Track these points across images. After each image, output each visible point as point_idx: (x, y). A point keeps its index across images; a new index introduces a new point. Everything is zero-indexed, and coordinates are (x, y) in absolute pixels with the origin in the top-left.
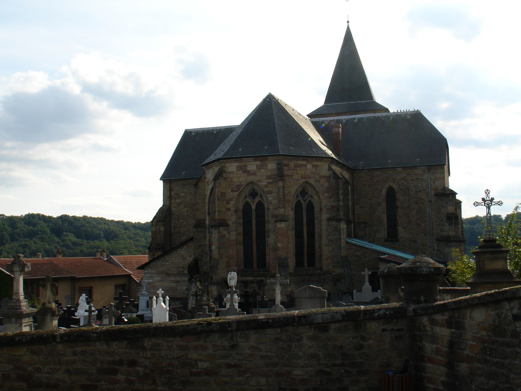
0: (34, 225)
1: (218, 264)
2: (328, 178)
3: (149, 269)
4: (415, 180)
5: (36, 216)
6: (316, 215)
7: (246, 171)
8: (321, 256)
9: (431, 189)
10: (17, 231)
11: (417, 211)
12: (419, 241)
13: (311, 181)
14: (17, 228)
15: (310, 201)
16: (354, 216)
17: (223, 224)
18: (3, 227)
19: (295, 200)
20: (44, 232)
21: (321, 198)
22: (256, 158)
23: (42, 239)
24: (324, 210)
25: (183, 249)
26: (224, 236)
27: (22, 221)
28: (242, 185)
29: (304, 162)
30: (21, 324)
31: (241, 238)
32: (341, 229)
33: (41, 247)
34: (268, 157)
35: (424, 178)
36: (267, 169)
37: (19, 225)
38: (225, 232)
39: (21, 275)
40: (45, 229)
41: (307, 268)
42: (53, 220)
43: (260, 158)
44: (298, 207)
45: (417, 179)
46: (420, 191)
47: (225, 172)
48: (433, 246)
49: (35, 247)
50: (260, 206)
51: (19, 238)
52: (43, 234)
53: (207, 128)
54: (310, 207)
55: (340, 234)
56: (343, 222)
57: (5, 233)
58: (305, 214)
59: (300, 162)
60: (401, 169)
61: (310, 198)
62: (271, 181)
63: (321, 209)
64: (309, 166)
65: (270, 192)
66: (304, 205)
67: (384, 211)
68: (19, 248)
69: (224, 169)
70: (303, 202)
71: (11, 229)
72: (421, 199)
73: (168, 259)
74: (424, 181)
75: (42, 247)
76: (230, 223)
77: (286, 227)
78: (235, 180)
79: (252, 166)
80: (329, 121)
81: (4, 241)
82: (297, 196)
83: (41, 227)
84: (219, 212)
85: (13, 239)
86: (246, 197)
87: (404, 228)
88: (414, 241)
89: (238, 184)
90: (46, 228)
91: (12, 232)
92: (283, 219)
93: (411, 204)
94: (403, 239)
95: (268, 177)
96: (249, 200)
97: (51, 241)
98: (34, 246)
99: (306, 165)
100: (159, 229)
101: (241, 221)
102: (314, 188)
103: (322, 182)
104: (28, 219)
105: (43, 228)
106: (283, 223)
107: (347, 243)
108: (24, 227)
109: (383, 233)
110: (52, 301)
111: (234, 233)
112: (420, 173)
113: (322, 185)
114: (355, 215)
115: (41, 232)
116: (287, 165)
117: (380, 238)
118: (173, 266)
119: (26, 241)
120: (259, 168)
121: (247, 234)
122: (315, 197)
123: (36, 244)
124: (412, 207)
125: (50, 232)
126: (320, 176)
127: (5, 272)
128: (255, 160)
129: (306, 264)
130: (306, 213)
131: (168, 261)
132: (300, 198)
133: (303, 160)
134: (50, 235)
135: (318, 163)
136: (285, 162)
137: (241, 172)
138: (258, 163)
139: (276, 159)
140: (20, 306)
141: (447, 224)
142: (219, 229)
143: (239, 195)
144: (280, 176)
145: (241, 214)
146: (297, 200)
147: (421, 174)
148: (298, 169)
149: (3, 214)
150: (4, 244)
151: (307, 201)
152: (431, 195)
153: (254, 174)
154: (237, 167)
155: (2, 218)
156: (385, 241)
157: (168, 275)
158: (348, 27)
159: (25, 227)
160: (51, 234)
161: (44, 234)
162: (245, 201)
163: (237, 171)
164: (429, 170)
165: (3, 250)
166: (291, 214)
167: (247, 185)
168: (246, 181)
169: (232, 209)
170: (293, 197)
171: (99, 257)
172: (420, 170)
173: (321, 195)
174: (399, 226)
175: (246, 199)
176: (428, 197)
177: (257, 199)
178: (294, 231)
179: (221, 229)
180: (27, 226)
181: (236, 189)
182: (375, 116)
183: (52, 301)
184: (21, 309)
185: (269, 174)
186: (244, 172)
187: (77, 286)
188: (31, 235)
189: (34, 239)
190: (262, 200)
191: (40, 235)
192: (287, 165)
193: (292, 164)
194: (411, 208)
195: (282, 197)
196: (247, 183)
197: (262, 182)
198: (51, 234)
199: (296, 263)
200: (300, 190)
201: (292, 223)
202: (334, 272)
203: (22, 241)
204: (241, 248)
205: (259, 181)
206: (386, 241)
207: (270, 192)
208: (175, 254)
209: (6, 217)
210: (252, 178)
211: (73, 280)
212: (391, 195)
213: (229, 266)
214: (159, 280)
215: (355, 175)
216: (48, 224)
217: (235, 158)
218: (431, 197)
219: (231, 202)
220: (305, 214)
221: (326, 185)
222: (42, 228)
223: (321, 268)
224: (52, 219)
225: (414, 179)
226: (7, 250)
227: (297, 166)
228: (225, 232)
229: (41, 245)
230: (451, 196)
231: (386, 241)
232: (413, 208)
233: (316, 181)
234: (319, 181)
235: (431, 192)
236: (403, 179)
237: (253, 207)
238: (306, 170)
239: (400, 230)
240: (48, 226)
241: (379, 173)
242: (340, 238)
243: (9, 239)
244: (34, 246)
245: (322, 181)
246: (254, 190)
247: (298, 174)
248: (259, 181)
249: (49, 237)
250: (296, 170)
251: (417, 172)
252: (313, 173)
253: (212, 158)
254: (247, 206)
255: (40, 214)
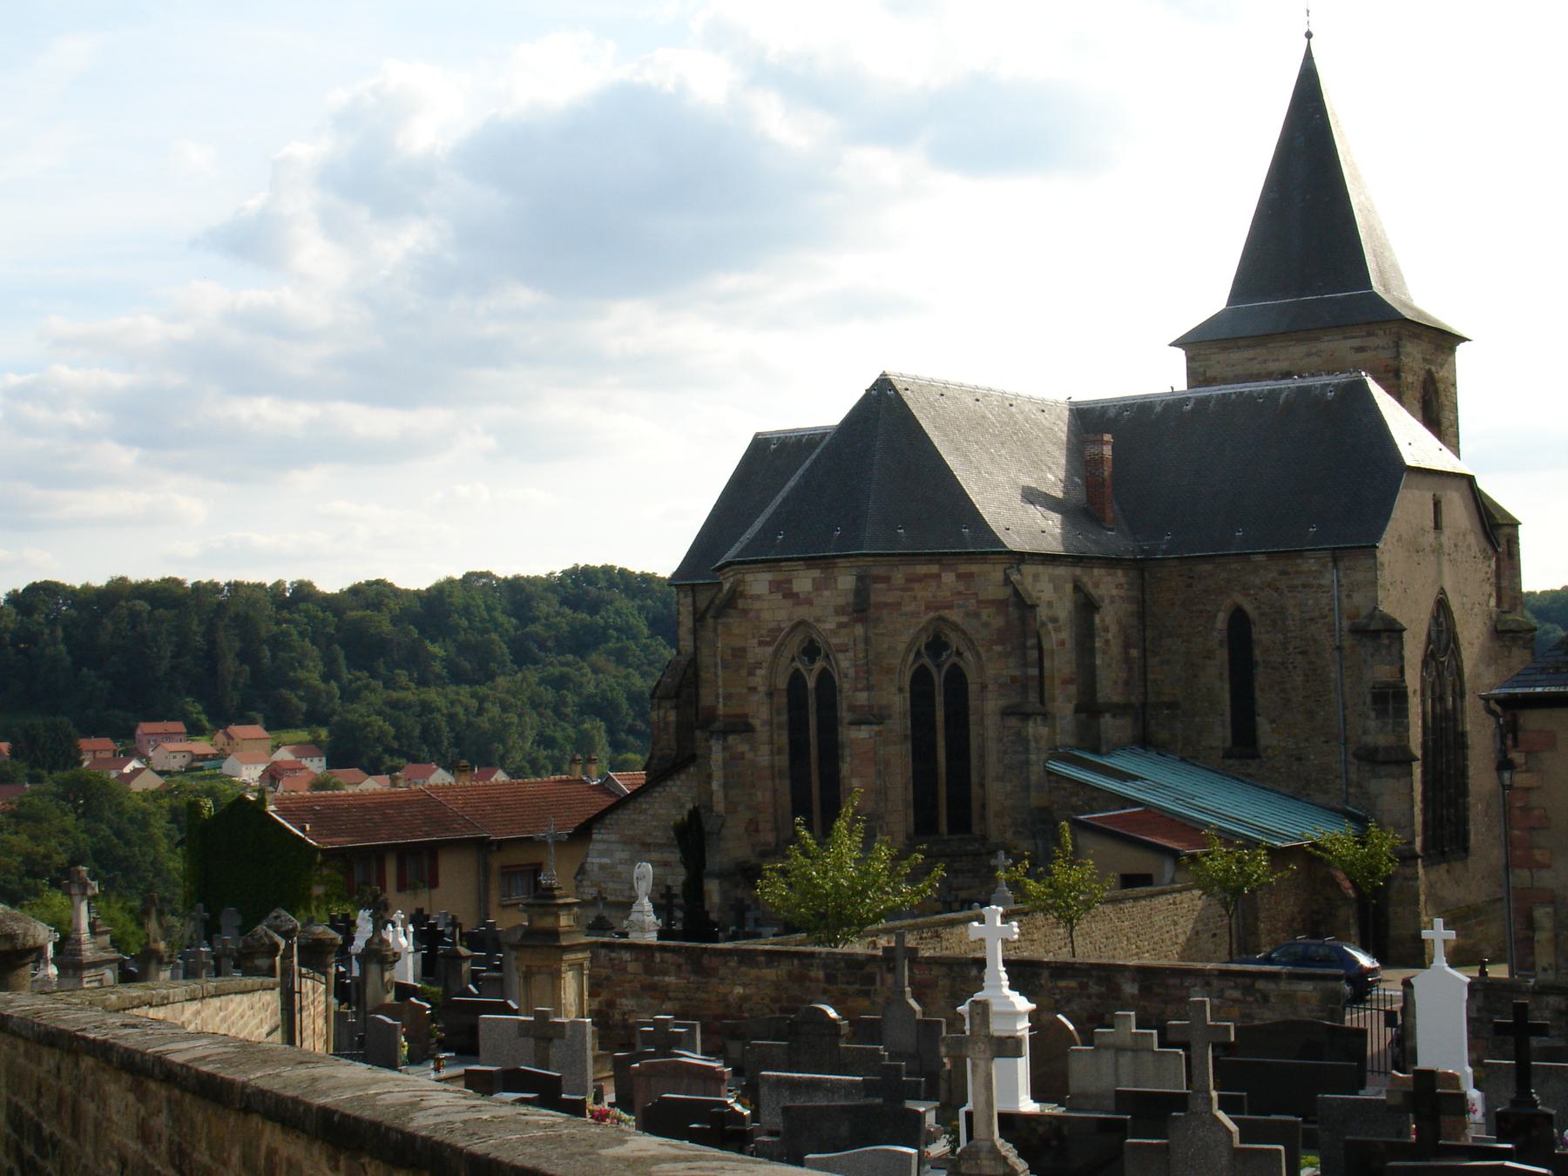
0: (594, 607)
1: (722, 825)
2: (1001, 605)
3: (602, 831)
4: (1300, 589)
5: (601, 575)
6: (973, 702)
7: (790, 595)
8: (983, 807)
9: (1340, 614)
10: (537, 628)
11: (1306, 675)
12: (1312, 757)
13: (954, 616)
14: (535, 619)
15: (955, 666)
16: (1146, 686)
17: (741, 726)
18: (487, 617)
19: (912, 665)
20: (626, 631)
21: (984, 656)
22: (811, 562)
23: (620, 657)
24: (990, 687)
25: (679, 783)
26: (742, 756)
27: (550, 595)
28: (780, 630)
29: (934, 569)
30: (81, 979)
31: (783, 761)
32: (1031, 737)
33: (615, 685)
34: (837, 561)
35: (1322, 582)
36: (836, 588)
37: (544, 608)
38: (744, 748)
39: (83, 900)
40: (631, 620)
41: (946, 837)
42: (657, 588)
43: (819, 562)
44: (921, 683)
45: (1304, 586)
46: (1312, 620)
47: (742, 595)
48: (1347, 772)
49: (597, 686)
50: (826, 681)
51: (542, 654)
52: (624, 637)
53: (810, 429)
54: (957, 680)
55: (1027, 751)
56: (1036, 720)
57: (495, 636)
58: (939, 700)
59: (922, 569)
60: (1261, 558)
61: (954, 659)
62: (844, 619)
63: (984, 687)
64: (949, 578)
65: (844, 649)
66: (939, 679)
67: (1221, 674)
68: (542, 688)
69: (742, 588)
70: (934, 670)
71: (514, 620)
72: (1315, 641)
73: (644, 806)
74: (1323, 592)
75: (619, 685)
76: (756, 723)
77: (870, 738)
78: (766, 616)
79: (803, 581)
80: (1120, 408)
81: (493, 665)
82: (918, 654)
83: (618, 613)
84: (728, 697)
85: (522, 656)
86: (793, 659)
87: (1273, 721)
88: (1299, 759)
89: (773, 625)
90: (633, 615)
91: (519, 633)
92: (872, 716)
93: (1289, 654)
94: (1269, 750)
95: (839, 611)
96: (800, 666)
97: (651, 664)
98: (592, 682)
99: (938, 576)
100: (665, 718)
101: (784, 718)
102: (964, 632)
103: (984, 617)
104: (571, 585)
105: (624, 617)
106: (863, 727)
107: (1050, 773)
108: (558, 614)
109: (1220, 733)
110: (159, 938)
111: (765, 749)
112: (1313, 569)
113: (986, 625)
114: (1149, 684)
115: (619, 630)
116: (887, 579)
117: (1211, 748)
118: (655, 823)
119: (567, 664)
120: (818, 586)
121: (798, 750)
122: (968, 655)
123: (601, 675)
124: (1292, 663)
125: (646, 631)
126: (979, 602)
127: (290, 831)
128: (809, 567)
129: (943, 826)
130: (942, 698)
131: (646, 810)
132: (926, 661)
133: (931, 562)
134: (648, 641)
135: (974, 568)
136: (880, 571)
137: (780, 596)
138: (816, 573)
139: (854, 564)
140: (80, 950)
141: (1373, 715)
142: (725, 740)
143: (776, 654)
144: (861, 608)
145: (783, 700)
146: (916, 665)
147: (1316, 571)
148: (917, 586)
149: (488, 572)
150: (491, 677)
151: (946, 667)
152: (1341, 630)
153: (809, 602)
154: (770, 582)
155: (485, 584)
156: (1223, 757)
157: (646, 846)
158: (1308, 57)
159: (563, 615)
160: (651, 637)
161: (627, 639)
162: (791, 670)
163: (771, 592)
164: (1335, 561)
165: (488, 696)
166: (898, 701)
167: (793, 629)
168: (790, 620)
169: (762, 689)
170: (904, 660)
171: (577, 777)
172: (1312, 561)
173: (981, 650)
174: (1259, 715)
175: (794, 664)
176: (1334, 636)
177: (819, 664)
178: (909, 745)
179: (731, 739)
180: (567, 611)
181: (768, 639)
182: (1242, 393)
183: (159, 938)
184: (81, 955)
185: (841, 601)
186: (785, 596)
187: (496, 861)
188: (581, 643)
189: (594, 657)
190: (828, 667)
191: (614, 640)
192: (887, 579)
193: (898, 577)
194: (1290, 666)
195: (862, 662)
196: (792, 623)
197: (824, 622)
198: (651, 637)
199: (917, 825)
200: (923, 640)
201: (900, 723)
202: (1015, 848)
203: (551, 664)
204: (785, 786)
205: (818, 620)
206: (1228, 755)
207: (844, 649)
208: (660, 793)
209: (498, 579)
210: (803, 612)
211: (483, 846)
212: (1240, 623)
213: (757, 830)
214: (626, 860)
215: (1146, 574)
216: (639, 602)
217: (763, 561)
218: (1341, 636)
219: (759, 672)
220: (939, 700)
221: (998, 622)
222: (620, 617)
223: (984, 838)
224: (654, 585)
225: (1297, 587)
226: (499, 695)
227: (911, 580)
228: (744, 748)
229: (615, 677)
230: (1384, 635)
231: (1228, 755)
232: (1295, 668)
233: (967, 615)
234: (977, 615)
235: (1340, 623)
236: (1269, 586)
237: (811, 683)
238: (939, 587)
239: (1264, 727)
240: (641, 609)
241: (1209, 567)
242: (1027, 762)
243: (508, 658)
244: (592, 682)
245: (985, 614)
246: (812, 642)
247: (915, 598)
248: (818, 620)
249: (647, 647)
250: (912, 589)
251: (1305, 567)
252: (959, 593)
253: (730, 555)
254: (797, 680)
255: (612, 568)
